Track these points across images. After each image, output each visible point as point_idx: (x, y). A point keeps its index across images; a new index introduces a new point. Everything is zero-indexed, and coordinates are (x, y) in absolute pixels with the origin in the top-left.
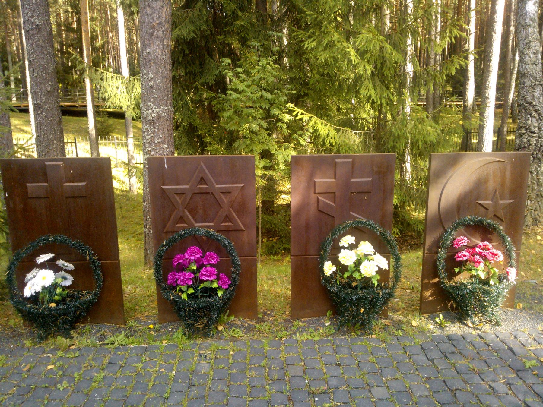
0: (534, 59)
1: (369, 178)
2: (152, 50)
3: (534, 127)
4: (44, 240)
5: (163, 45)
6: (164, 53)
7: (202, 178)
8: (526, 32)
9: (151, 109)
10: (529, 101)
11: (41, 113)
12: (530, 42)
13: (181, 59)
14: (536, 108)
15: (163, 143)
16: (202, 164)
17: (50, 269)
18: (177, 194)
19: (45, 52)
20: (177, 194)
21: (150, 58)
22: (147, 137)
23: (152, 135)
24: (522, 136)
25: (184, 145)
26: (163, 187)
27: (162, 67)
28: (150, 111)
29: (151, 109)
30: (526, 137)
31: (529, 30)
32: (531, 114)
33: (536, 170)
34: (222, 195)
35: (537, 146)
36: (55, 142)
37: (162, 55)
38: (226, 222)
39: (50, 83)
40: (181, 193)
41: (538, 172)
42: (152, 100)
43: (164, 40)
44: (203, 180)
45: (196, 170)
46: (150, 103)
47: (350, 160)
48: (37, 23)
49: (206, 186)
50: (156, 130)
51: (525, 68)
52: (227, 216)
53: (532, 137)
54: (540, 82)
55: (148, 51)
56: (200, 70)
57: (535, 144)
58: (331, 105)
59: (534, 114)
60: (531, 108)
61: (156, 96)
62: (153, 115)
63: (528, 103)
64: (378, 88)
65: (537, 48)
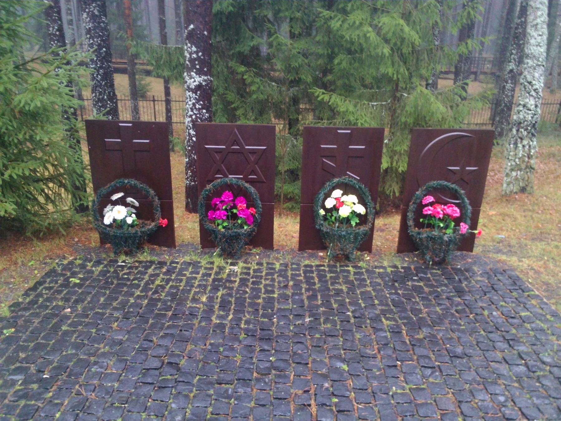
0: (539, 41)
3: (531, 105)
4: (121, 182)
10: (529, 80)
12: (537, 24)
13: (255, 210)
14: (535, 87)
15: (203, 108)
16: (236, 130)
17: (122, 205)
22: (190, 103)
24: (519, 113)
25: (219, 110)
32: (529, 93)
33: (528, 144)
41: (530, 146)
45: (446, 410)
52: (253, 171)
53: (528, 114)
54: (542, 62)
56: (236, 38)
59: (533, 93)
60: (530, 87)
63: (528, 82)
64: (396, 65)
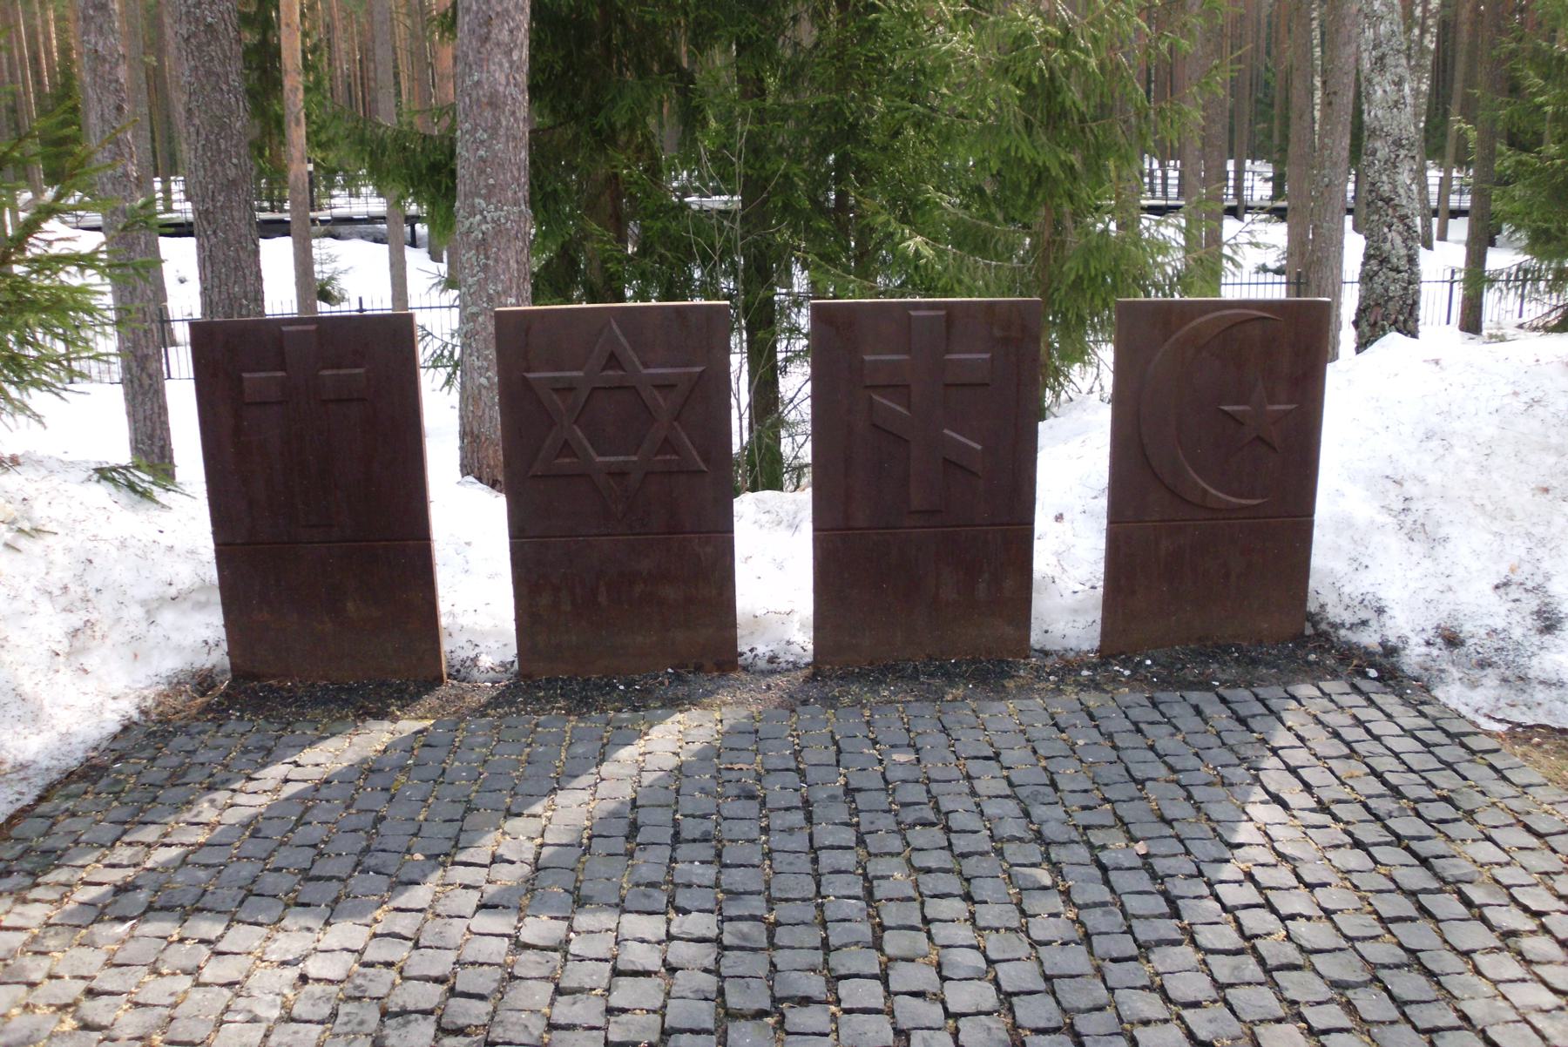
1: (986, 352)
2: (485, 75)
5: (512, 63)
6: (512, 81)
7: (566, 442)
8: (1375, 32)
9: (481, 213)
11: (215, 232)
18: (557, 390)
19: (225, 87)
20: (557, 390)
21: (481, 93)
22: (470, 281)
23: (482, 275)
26: (526, 374)
27: (507, 113)
28: (478, 217)
29: (481, 213)
30: (1380, 281)
31: (1382, 27)
34: (656, 392)
35: (1404, 302)
36: (245, 302)
37: (508, 83)
38: (666, 454)
39: (235, 161)
40: (567, 389)
42: (483, 192)
43: (511, 51)
44: (613, 361)
46: (477, 200)
47: (943, 313)
48: (209, 20)
49: (621, 373)
50: (491, 263)
51: (1376, 116)
52: (666, 440)
55: (476, 78)
57: (1401, 297)
58: (1092, 700)
60: (1390, 211)
61: (491, 181)
62: (484, 227)
65: (1399, 70)
